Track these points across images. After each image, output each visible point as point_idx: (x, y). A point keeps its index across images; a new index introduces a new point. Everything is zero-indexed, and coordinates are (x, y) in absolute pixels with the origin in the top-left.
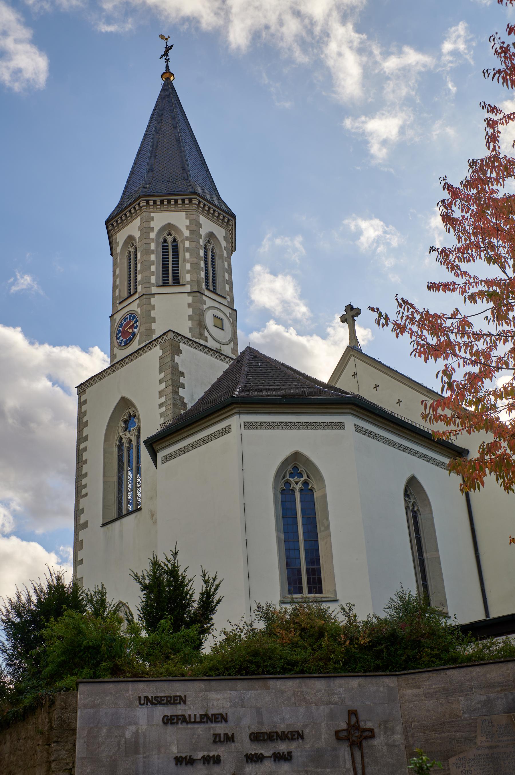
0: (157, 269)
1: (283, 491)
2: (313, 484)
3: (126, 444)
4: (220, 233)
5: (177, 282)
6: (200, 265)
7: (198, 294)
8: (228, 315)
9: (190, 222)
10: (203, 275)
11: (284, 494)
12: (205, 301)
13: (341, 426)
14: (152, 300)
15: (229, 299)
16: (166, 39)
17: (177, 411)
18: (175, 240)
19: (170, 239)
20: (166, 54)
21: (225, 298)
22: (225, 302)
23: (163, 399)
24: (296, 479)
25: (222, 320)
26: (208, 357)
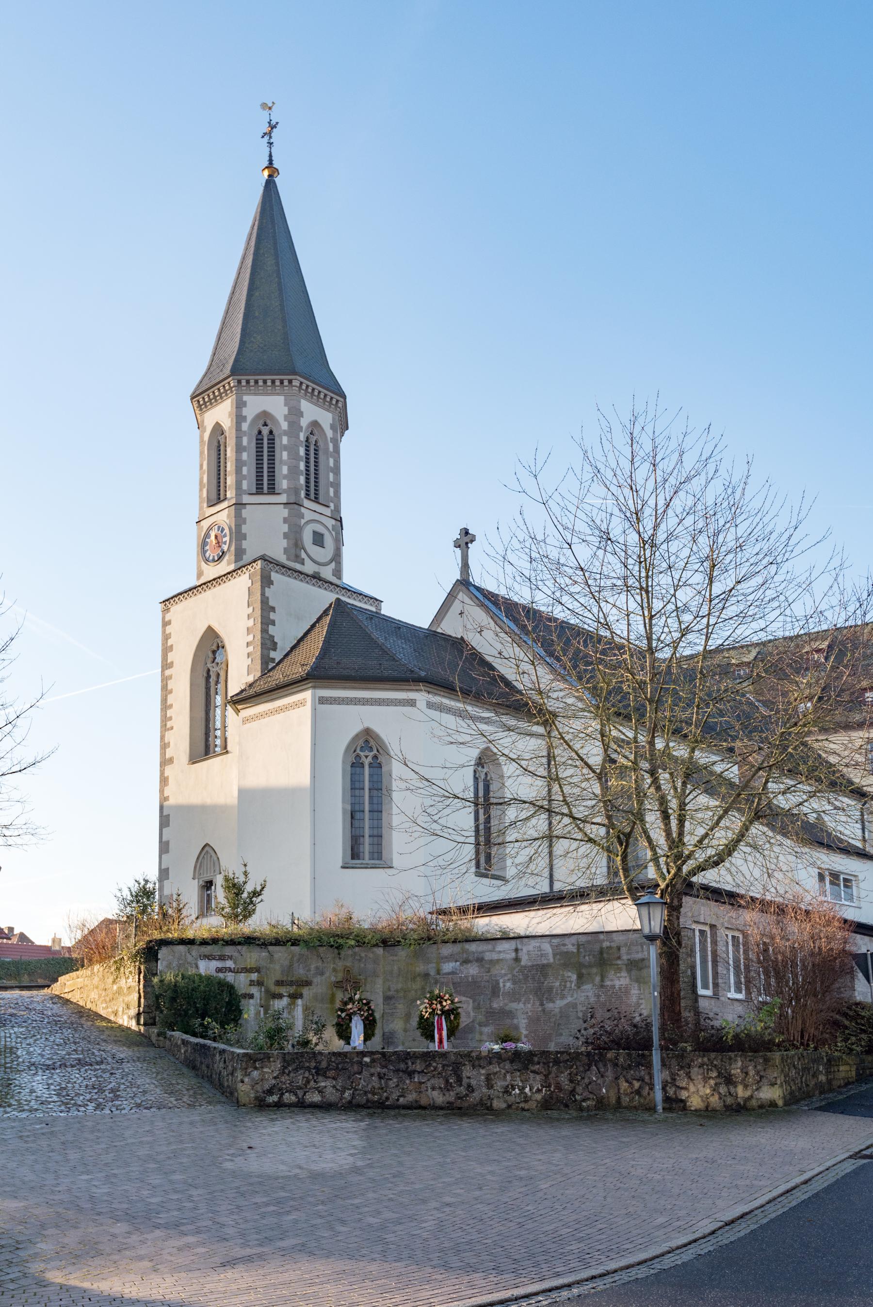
0: (249, 471)
1: (353, 765)
2: (382, 759)
4: (326, 418)
5: (272, 491)
7: (296, 506)
8: (331, 528)
10: (302, 480)
11: (357, 765)
13: (412, 703)
14: (243, 511)
16: (270, 108)
17: (266, 652)
18: (271, 432)
19: (265, 431)
21: (328, 507)
22: (327, 511)
24: (367, 753)
25: (322, 535)
26: (303, 585)
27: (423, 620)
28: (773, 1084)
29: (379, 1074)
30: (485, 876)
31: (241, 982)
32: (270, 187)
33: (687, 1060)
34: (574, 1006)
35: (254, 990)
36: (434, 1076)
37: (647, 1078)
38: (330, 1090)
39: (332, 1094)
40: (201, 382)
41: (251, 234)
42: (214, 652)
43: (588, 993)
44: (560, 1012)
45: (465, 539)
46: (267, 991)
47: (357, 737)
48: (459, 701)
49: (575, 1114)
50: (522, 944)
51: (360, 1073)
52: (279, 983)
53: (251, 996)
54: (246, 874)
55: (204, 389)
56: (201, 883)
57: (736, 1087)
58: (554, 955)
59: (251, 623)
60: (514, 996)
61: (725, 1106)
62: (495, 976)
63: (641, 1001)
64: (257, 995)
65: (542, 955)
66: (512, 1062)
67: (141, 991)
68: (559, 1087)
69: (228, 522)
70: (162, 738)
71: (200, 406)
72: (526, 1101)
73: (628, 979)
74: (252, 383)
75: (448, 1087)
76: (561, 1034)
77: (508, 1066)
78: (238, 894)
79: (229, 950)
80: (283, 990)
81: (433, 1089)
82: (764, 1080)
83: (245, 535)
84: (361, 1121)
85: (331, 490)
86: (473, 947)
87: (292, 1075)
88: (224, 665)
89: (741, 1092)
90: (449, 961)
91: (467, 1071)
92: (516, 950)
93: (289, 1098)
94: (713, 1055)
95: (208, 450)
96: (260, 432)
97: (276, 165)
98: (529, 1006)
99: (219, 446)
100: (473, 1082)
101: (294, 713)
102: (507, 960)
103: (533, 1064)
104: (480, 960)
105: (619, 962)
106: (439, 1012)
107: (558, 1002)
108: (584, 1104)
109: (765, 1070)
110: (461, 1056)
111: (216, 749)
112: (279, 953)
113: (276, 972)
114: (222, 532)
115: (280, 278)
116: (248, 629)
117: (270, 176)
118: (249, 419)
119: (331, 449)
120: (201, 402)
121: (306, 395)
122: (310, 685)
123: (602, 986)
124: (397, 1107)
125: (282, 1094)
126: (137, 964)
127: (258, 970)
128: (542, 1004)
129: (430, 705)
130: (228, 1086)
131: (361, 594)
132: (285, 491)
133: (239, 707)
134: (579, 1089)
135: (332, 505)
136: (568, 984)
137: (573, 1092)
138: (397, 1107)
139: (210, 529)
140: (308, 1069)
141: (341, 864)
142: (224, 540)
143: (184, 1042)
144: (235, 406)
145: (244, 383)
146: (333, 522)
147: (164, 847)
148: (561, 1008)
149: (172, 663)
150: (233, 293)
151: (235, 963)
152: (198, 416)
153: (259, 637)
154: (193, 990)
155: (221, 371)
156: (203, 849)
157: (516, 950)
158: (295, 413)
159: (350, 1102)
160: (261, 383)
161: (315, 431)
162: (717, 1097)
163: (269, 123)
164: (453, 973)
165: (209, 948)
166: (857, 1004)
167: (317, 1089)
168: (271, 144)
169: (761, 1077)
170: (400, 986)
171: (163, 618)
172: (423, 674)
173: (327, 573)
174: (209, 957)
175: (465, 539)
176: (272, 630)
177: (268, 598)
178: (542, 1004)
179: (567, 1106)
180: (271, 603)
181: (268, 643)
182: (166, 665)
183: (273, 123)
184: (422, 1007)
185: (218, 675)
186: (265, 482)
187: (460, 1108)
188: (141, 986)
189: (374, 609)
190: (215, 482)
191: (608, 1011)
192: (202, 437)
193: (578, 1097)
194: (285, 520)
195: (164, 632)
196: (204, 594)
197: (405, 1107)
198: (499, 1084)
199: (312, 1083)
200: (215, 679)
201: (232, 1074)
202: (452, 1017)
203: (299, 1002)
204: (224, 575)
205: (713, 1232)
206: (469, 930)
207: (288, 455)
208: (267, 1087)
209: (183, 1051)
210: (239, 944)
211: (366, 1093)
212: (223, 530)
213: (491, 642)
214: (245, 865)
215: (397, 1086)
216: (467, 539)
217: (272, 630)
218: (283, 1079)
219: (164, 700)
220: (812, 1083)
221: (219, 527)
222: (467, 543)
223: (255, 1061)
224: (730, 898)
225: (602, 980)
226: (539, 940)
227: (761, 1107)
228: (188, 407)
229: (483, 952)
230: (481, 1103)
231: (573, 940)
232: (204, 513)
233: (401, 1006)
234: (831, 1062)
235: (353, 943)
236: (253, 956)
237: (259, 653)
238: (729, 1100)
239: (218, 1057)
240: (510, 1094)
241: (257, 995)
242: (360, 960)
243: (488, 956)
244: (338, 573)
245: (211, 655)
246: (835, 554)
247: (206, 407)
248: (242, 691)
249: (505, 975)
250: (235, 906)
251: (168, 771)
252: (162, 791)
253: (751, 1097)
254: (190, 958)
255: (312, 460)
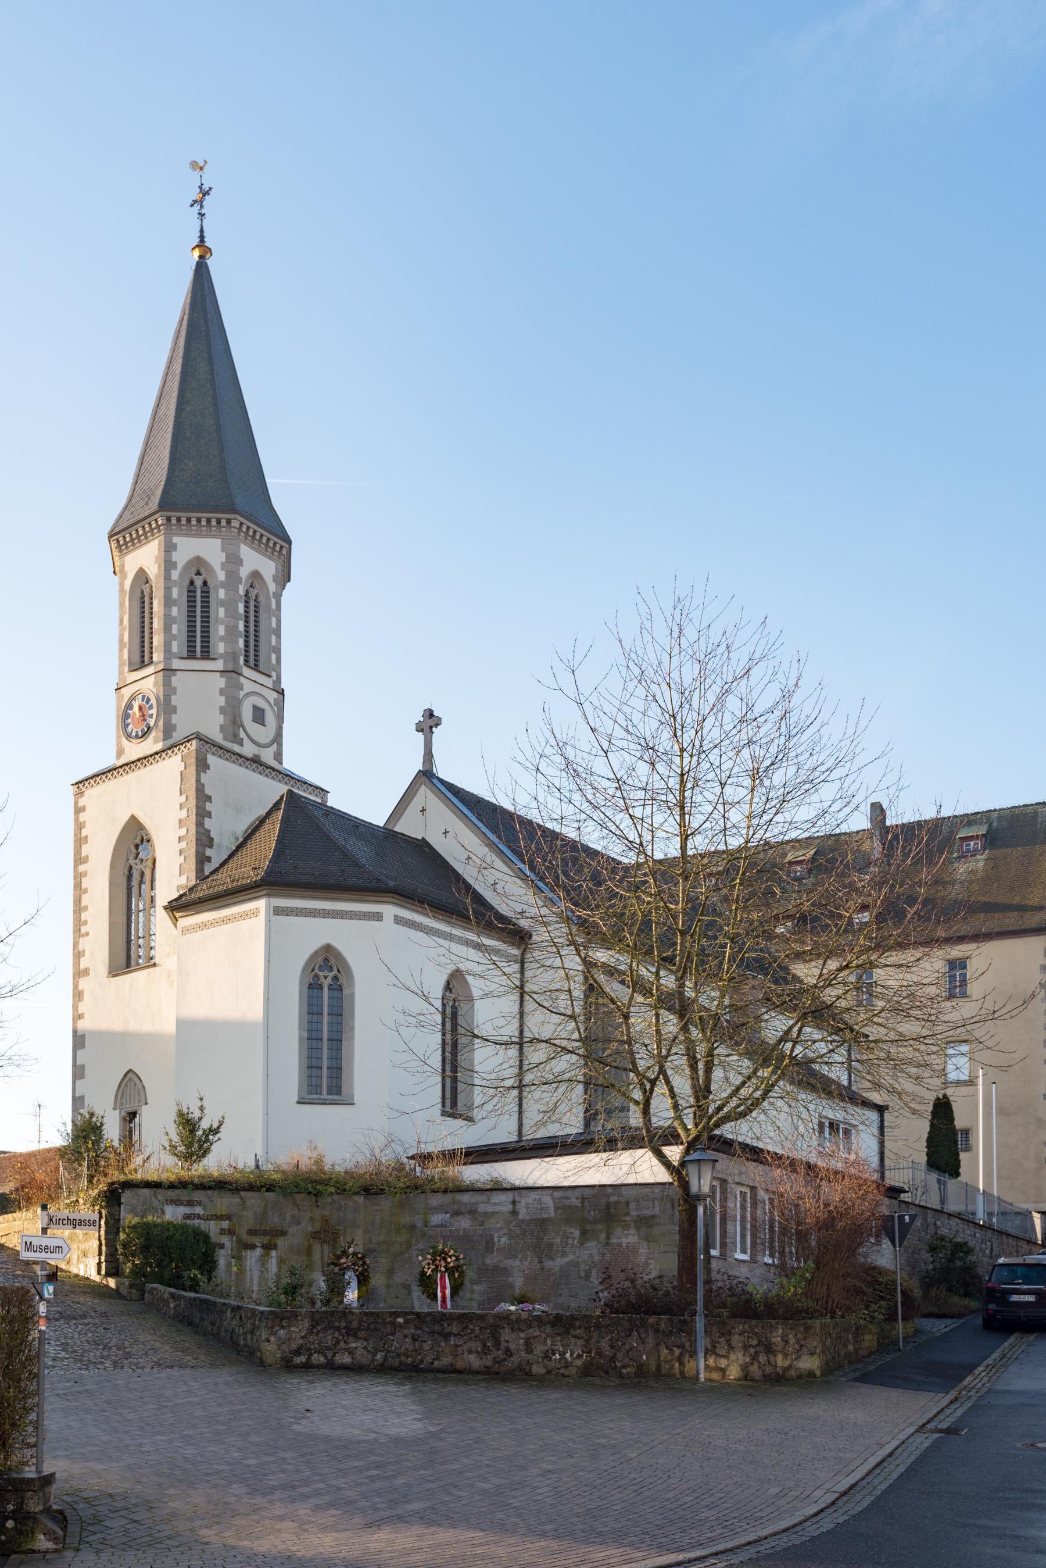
0: (179, 629)
1: (310, 987)
2: (342, 980)
3: (136, 876)
4: (268, 568)
5: (206, 655)
6: (237, 628)
7: (234, 675)
9: (227, 557)
10: (241, 643)
11: (313, 987)
12: (242, 685)
13: (378, 917)
14: (173, 678)
15: (274, 678)
16: (201, 168)
17: (201, 849)
18: (205, 583)
19: (198, 582)
20: (199, 202)
21: (270, 676)
22: (268, 682)
23: (183, 832)
24: (326, 973)
25: (263, 711)
26: (242, 770)
27: (377, 816)
28: (812, 1354)
29: (413, 1335)
30: (453, 1116)
31: (212, 1228)
32: (202, 271)
33: (728, 1327)
34: (575, 1264)
35: (225, 1240)
36: (470, 1339)
37: (687, 1345)
38: (360, 1351)
39: (363, 1355)
40: (121, 517)
41: (179, 331)
42: (137, 846)
43: (593, 1249)
44: (561, 1271)
45: (429, 722)
46: (239, 1241)
47: (315, 955)
48: (427, 915)
49: (618, 1381)
50: (520, 1195)
51: (393, 1334)
52: (252, 1232)
53: (222, 1246)
54: (202, 1108)
55: (125, 525)
56: (123, 1114)
57: (775, 1356)
58: (556, 1209)
59: (183, 814)
60: (510, 1252)
61: (764, 1376)
62: (490, 1229)
63: (649, 1261)
64: (228, 1244)
65: (542, 1209)
66: (553, 1326)
67: (103, 1238)
68: (599, 1353)
69: (154, 690)
70: (76, 945)
71: (119, 546)
72: (566, 1367)
73: (636, 1237)
74: (184, 521)
75: (486, 1351)
76: (561, 1295)
77: (548, 1329)
78: (192, 1131)
79: (198, 1195)
80: (257, 1240)
81: (470, 1352)
82: (804, 1350)
83: (175, 707)
84: (402, 1384)
85: (274, 656)
86: (465, 1198)
87: (321, 1335)
88: (150, 863)
89: (780, 1361)
90: (438, 1213)
91: (506, 1335)
92: (514, 1203)
93: (317, 1359)
94: (754, 1322)
95: (130, 601)
96: (192, 583)
97: (208, 243)
98: (527, 1263)
99: (143, 597)
100: (512, 1346)
101: (243, 925)
102: (502, 1213)
103: (575, 1328)
104: (473, 1212)
105: (627, 1218)
106: (443, 1269)
107: (558, 1260)
108: (624, 1371)
109: (805, 1339)
110: (500, 1319)
111: (140, 961)
112: (253, 1199)
113: (248, 1219)
114: (147, 702)
115: (215, 391)
116: (180, 821)
117: (200, 257)
118: (180, 566)
119: (274, 606)
120: (122, 542)
121: (246, 539)
122: (264, 892)
123: (607, 1244)
124: (431, 1370)
125: (311, 1355)
126: (97, 1208)
127: (228, 1217)
128: (540, 1262)
129: (398, 920)
130: (246, 1345)
131: (305, 783)
132: (221, 656)
133: (178, 915)
134: (620, 1355)
135: (274, 674)
136: (570, 1241)
137: (613, 1358)
138: (431, 1370)
139: (133, 698)
140: (338, 1329)
141: (296, 1099)
142: (151, 712)
143: (173, 1296)
144: (163, 549)
145: (174, 521)
146: (275, 695)
147: (78, 1072)
148: (561, 1266)
149: (87, 857)
150: (158, 406)
151: (204, 1209)
152: (116, 559)
153: (194, 831)
154: (167, 1238)
155: (147, 504)
156: (125, 1075)
157: (514, 1203)
158: (233, 561)
159: (382, 1365)
160: (194, 522)
161: (256, 584)
162: (756, 1366)
163: (200, 188)
164: (441, 1226)
165: (177, 1192)
166: (874, 1268)
167: (347, 1350)
168: (202, 215)
169: (801, 1346)
170: (382, 1238)
171: (76, 803)
172: (391, 883)
173: (267, 756)
174: (177, 1202)
175: (429, 722)
176: (208, 823)
177: (203, 786)
178: (540, 1262)
179: (606, 1372)
180: (207, 792)
181: (204, 840)
182: (80, 860)
183: (206, 187)
184: (424, 1264)
185: (142, 874)
186: (197, 645)
187: (497, 1373)
188: (103, 1232)
189: (319, 801)
190: (137, 641)
191: (622, 1271)
192: (121, 585)
193: (618, 1364)
194: (222, 692)
195: (77, 819)
196: (125, 777)
197: (439, 1371)
198: (539, 1349)
199: (342, 1344)
200: (139, 878)
201: (252, 1332)
202: (457, 1275)
203: (274, 1253)
204: (151, 756)
205: (833, 1503)
206: (454, 1179)
207: (226, 612)
208: (294, 1347)
209: (172, 1306)
210: (210, 1188)
211: (398, 1355)
212: (148, 700)
213: (461, 845)
214: (201, 1099)
215: (432, 1348)
216: (430, 722)
217: (208, 823)
218: (311, 1339)
219: (78, 901)
220: (842, 1354)
221: (144, 697)
222: (431, 727)
223: (282, 1320)
224: (755, 1154)
225: (608, 1238)
226: (540, 1192)
227: (800, 1377)
228: (103, 547)
229: (477, 1203)
230: (520, 1368)
231: (577, 1193)
232: (125, 678)
233: (383, 1260)
234: (859, 1331)
235: (333, 1190)
236: (224, 1202)
237: (193, 850)
238: (768, 1370)
239: (229, 1313)
240: (551, 1359)
241: (228, 1244)
242: (339, 1210)
243: (482, 1208)
244: (279, 756)
245: (133, 850)
246: (888, 770)
247: (127, 548)
248: (181, 896)
249: (501, 1229)
250: (189, 1146)
251: (83, 983)
252: (75, 1007)
253: (790, 1367)
254: (155, 1203)
255: (252, 619)
